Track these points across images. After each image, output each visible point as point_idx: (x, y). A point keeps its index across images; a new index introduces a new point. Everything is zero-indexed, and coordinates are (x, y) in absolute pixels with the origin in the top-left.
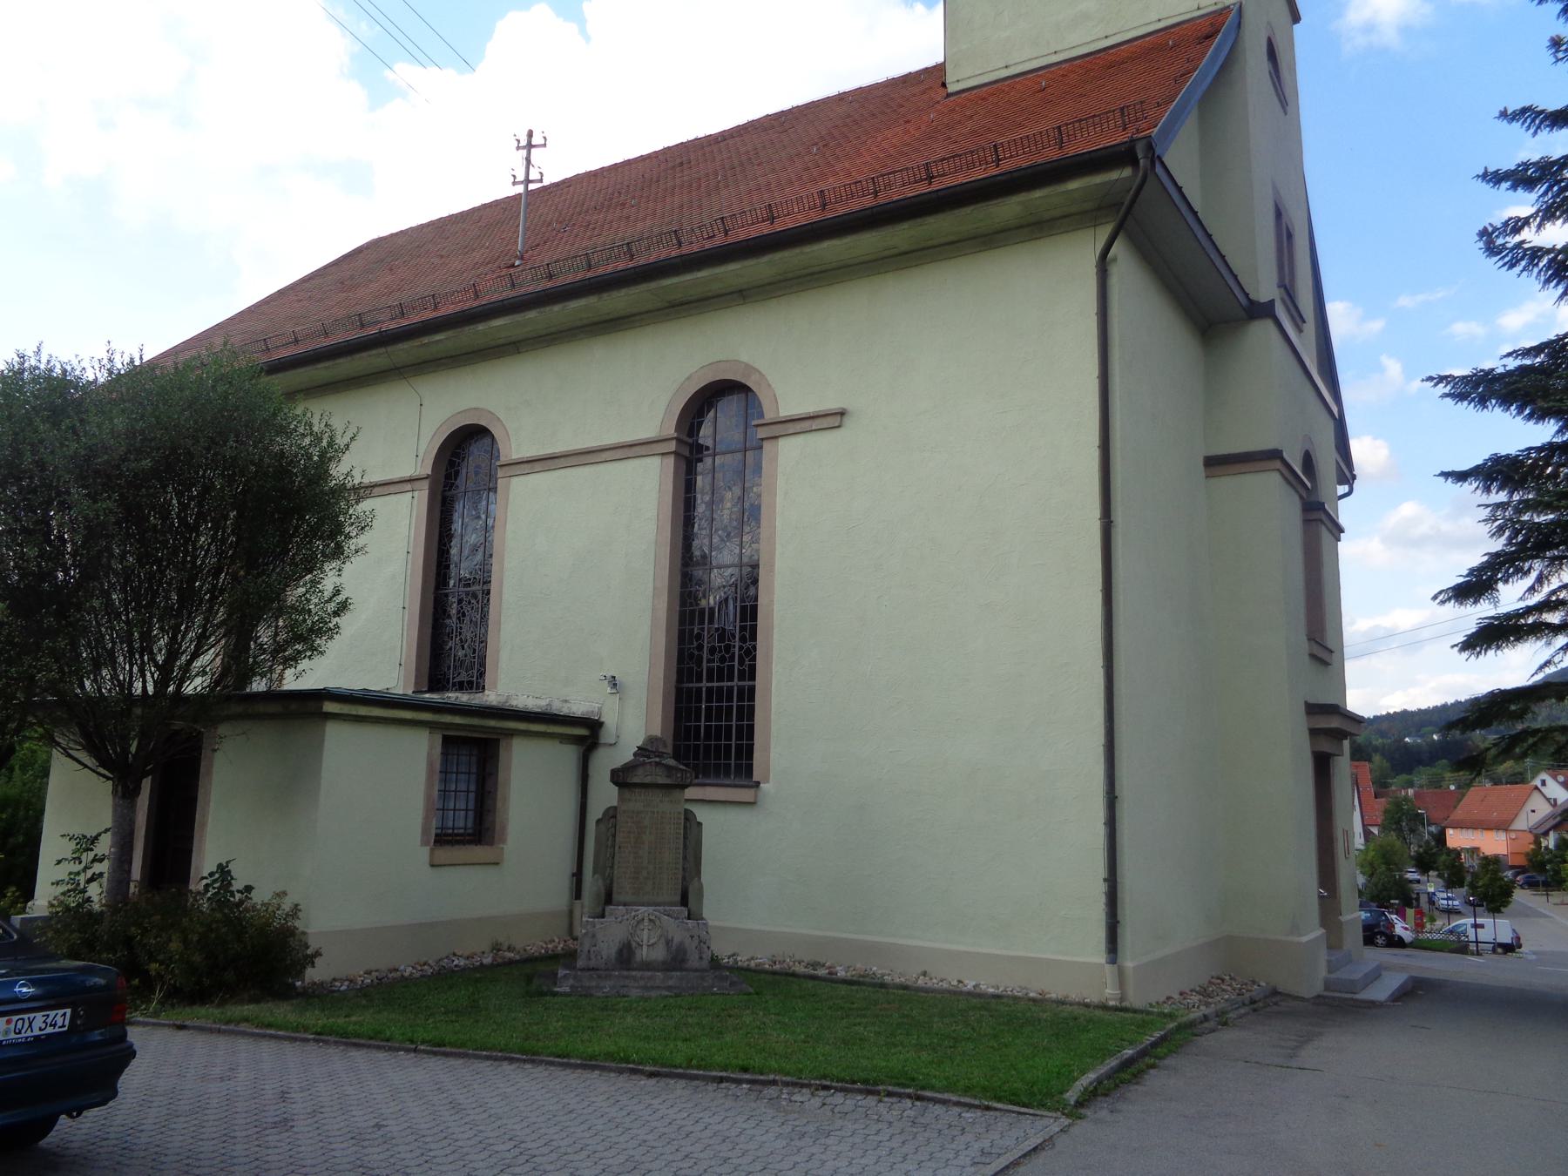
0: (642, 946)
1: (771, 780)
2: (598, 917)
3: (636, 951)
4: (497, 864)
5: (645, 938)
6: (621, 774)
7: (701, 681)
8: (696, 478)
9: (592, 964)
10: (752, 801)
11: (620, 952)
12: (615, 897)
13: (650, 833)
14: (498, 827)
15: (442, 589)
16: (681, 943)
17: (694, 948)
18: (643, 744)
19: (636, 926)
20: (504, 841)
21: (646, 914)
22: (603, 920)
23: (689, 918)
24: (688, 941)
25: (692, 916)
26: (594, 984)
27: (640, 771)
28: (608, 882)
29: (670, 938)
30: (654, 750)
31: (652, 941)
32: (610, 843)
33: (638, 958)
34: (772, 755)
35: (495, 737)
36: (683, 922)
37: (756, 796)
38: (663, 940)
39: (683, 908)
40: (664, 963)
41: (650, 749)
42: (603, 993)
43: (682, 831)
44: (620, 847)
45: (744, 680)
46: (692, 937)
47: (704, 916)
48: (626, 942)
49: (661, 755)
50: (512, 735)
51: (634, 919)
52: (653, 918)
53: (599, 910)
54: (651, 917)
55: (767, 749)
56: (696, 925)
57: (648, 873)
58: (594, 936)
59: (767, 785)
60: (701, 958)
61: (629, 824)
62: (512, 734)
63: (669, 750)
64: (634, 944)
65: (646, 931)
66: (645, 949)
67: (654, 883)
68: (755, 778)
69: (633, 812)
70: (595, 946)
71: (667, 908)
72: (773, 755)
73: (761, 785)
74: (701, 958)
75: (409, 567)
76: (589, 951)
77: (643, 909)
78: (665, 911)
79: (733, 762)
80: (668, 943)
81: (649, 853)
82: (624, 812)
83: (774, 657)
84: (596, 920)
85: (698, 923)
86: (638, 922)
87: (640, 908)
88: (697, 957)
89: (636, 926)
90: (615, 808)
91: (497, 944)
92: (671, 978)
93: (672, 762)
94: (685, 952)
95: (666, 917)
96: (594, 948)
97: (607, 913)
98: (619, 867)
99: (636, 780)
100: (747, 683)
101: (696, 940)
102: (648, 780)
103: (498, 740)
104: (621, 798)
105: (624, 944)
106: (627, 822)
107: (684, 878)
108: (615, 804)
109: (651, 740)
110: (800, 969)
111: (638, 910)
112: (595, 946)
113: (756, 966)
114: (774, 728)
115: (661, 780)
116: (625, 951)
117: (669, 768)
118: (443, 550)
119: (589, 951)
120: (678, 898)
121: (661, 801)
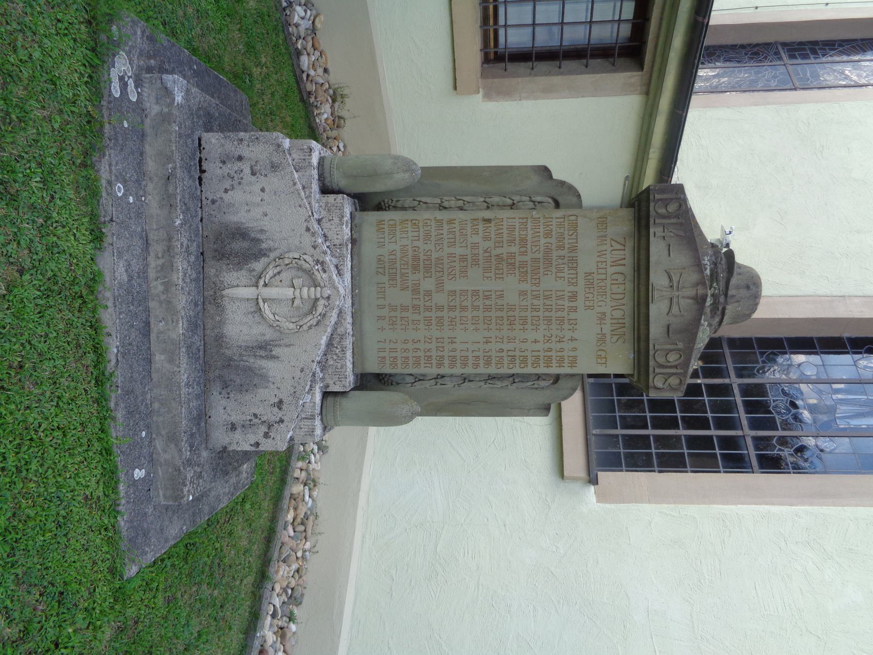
0: (256, 286)
1: (601, 505)
2: (321, 177)
3: (244, 272)
4: (455, 88)
5: (271, 292)
6: (672, 208)
7: (740, 376)
8: (848, 353)
9: (213, 168)
10: (566, 473)
11: (241, 233)
12: (372, 216)
13: (523, 293)
14: (508, 82)
15: (783, 49)
16: (264, 378)
17: (253, 411)
18: (740, 266)
19: (300, 268)
20: (488, 96)
21: (327, 292)
22: (315, 187)
23: (326, 395)
24: (268, 394)
25: (330, 400)
26: (151, 165)
27: (681, 258)
28: (408, 202)
29: (276, 351)
30: (731, 292)
31: (266, 308)
32: (496, 199)
33: (231, 277)
34: (647, 507)
35: (646, 67)
36: (313, 382)
37: (575, 479)
38: (269, 334)
39: (351, 378)
40: (220, 338)
41: (734, 281)
42: (110, 183)
43: (529, 370)
44: (489, 221)
45: (757, 448)
46: (280, 404)
47: (337, 430)
48: (264, 246)
49: (718, 310)
50: (647, 93)
51: (317, 262)
52: (320, 309)
53: (338, 179)
54: (322, 302)
55: (655, 497)
56: (309, 412)
57: (428, 293)
58: (274, 167)
59: (594, 499)
60: (233, 427)
61: (543, 241)
62: (651, 92)
63: (729, 331)
64: (258, 266)
65: (289, 292)
66: (249, 292)
67: (404, 308)
68: (603, 476)
69: (574, 249)
70: (253, 174)
71: (348, 342)
72: (647, 509)
73: (592, 488)
74: (233, 427)
75: (809, 7)
76: (240, 158)
77: (344, 284)
78: (342, 337)
79: (620, 432)
80: (264, 348)
81: (475, 293)
82: (574, 227)
83: (824, 510)
84: (315, 173)
85: (312, 417)
86: (309, 273)
87: (348, 276)
88: (234, 418)
89: (300, 268)
90: (579, 205)
91: (342, 96)
92: (171, 361)
93: (703, 337)
94: (242, 389)
95: (324, 341)
96: (247, 171)
97: (331, 198)
98: (439, 222)
99: (657, 248)
100: (752, 453)
101: (272, 414)
102: (657, 279)
103: (641, 68)
104: (602, 216)
105: (258, 241)
106: (548, 235)
107: (419, 378)
108: (586, 200)
109: (753, 284)
110: (282, 574)
111: (340, 274)
112: (253, 174)
113: (292, 497)
114: (693, 510)
115: (658, 310)
116: (239, 245)
117: (690, 331)
118: (834, 45)
119: (240, 158)
120: (373, 367)
121: (602, 317)
